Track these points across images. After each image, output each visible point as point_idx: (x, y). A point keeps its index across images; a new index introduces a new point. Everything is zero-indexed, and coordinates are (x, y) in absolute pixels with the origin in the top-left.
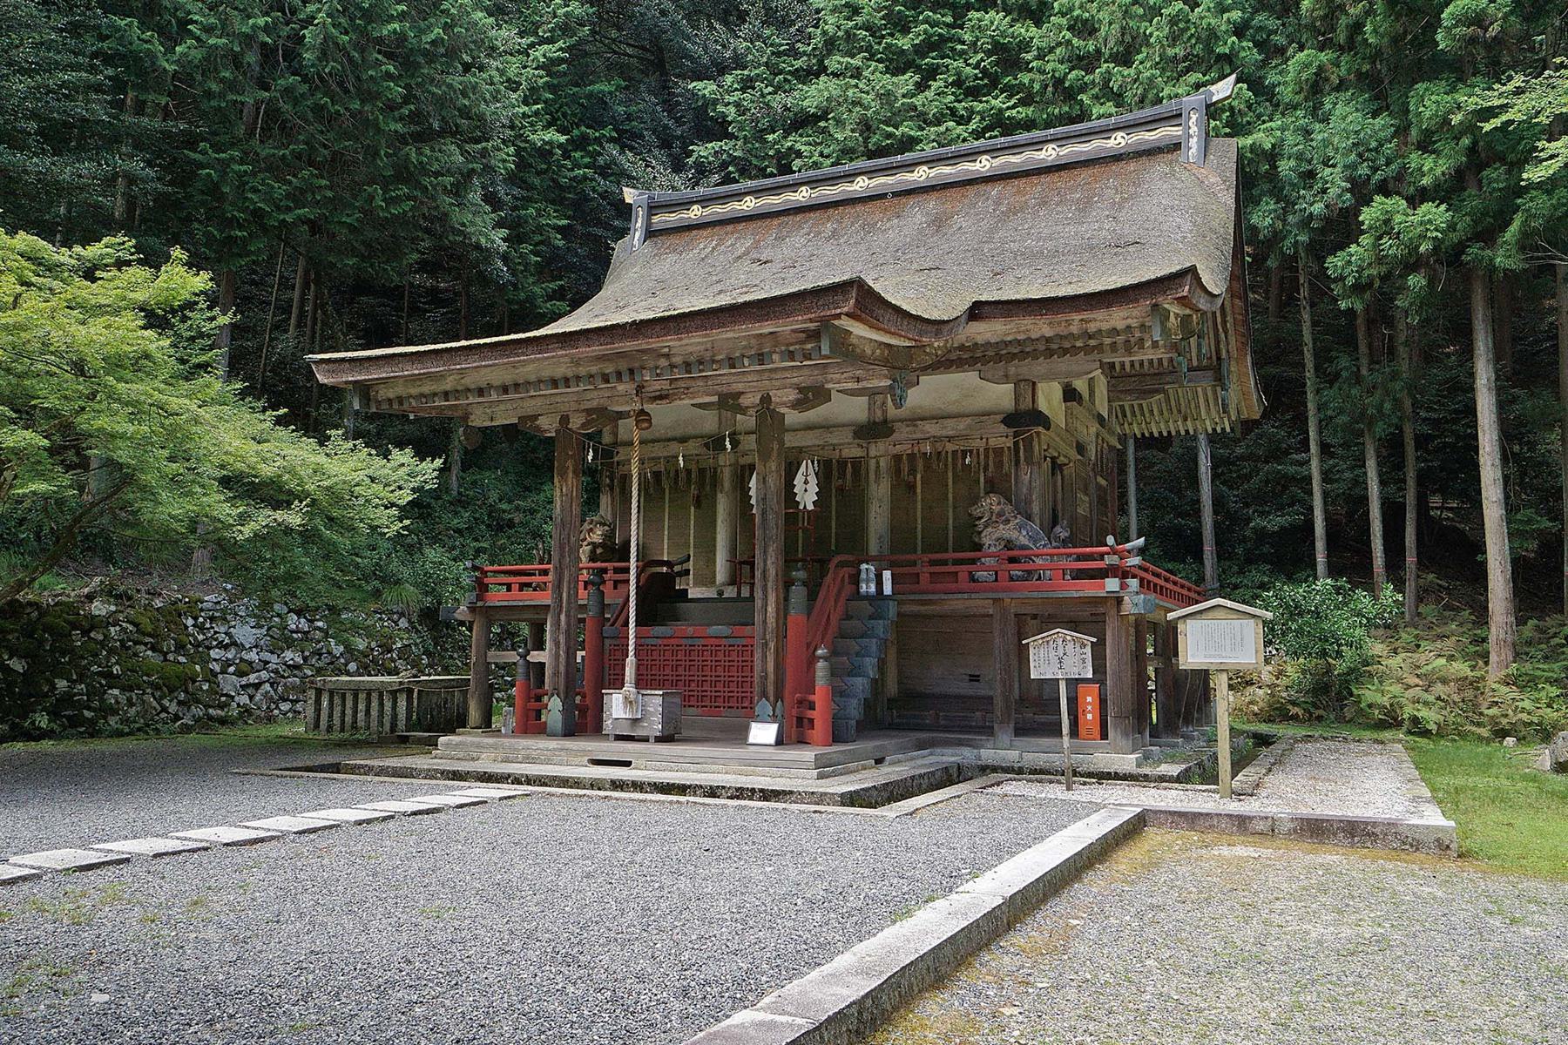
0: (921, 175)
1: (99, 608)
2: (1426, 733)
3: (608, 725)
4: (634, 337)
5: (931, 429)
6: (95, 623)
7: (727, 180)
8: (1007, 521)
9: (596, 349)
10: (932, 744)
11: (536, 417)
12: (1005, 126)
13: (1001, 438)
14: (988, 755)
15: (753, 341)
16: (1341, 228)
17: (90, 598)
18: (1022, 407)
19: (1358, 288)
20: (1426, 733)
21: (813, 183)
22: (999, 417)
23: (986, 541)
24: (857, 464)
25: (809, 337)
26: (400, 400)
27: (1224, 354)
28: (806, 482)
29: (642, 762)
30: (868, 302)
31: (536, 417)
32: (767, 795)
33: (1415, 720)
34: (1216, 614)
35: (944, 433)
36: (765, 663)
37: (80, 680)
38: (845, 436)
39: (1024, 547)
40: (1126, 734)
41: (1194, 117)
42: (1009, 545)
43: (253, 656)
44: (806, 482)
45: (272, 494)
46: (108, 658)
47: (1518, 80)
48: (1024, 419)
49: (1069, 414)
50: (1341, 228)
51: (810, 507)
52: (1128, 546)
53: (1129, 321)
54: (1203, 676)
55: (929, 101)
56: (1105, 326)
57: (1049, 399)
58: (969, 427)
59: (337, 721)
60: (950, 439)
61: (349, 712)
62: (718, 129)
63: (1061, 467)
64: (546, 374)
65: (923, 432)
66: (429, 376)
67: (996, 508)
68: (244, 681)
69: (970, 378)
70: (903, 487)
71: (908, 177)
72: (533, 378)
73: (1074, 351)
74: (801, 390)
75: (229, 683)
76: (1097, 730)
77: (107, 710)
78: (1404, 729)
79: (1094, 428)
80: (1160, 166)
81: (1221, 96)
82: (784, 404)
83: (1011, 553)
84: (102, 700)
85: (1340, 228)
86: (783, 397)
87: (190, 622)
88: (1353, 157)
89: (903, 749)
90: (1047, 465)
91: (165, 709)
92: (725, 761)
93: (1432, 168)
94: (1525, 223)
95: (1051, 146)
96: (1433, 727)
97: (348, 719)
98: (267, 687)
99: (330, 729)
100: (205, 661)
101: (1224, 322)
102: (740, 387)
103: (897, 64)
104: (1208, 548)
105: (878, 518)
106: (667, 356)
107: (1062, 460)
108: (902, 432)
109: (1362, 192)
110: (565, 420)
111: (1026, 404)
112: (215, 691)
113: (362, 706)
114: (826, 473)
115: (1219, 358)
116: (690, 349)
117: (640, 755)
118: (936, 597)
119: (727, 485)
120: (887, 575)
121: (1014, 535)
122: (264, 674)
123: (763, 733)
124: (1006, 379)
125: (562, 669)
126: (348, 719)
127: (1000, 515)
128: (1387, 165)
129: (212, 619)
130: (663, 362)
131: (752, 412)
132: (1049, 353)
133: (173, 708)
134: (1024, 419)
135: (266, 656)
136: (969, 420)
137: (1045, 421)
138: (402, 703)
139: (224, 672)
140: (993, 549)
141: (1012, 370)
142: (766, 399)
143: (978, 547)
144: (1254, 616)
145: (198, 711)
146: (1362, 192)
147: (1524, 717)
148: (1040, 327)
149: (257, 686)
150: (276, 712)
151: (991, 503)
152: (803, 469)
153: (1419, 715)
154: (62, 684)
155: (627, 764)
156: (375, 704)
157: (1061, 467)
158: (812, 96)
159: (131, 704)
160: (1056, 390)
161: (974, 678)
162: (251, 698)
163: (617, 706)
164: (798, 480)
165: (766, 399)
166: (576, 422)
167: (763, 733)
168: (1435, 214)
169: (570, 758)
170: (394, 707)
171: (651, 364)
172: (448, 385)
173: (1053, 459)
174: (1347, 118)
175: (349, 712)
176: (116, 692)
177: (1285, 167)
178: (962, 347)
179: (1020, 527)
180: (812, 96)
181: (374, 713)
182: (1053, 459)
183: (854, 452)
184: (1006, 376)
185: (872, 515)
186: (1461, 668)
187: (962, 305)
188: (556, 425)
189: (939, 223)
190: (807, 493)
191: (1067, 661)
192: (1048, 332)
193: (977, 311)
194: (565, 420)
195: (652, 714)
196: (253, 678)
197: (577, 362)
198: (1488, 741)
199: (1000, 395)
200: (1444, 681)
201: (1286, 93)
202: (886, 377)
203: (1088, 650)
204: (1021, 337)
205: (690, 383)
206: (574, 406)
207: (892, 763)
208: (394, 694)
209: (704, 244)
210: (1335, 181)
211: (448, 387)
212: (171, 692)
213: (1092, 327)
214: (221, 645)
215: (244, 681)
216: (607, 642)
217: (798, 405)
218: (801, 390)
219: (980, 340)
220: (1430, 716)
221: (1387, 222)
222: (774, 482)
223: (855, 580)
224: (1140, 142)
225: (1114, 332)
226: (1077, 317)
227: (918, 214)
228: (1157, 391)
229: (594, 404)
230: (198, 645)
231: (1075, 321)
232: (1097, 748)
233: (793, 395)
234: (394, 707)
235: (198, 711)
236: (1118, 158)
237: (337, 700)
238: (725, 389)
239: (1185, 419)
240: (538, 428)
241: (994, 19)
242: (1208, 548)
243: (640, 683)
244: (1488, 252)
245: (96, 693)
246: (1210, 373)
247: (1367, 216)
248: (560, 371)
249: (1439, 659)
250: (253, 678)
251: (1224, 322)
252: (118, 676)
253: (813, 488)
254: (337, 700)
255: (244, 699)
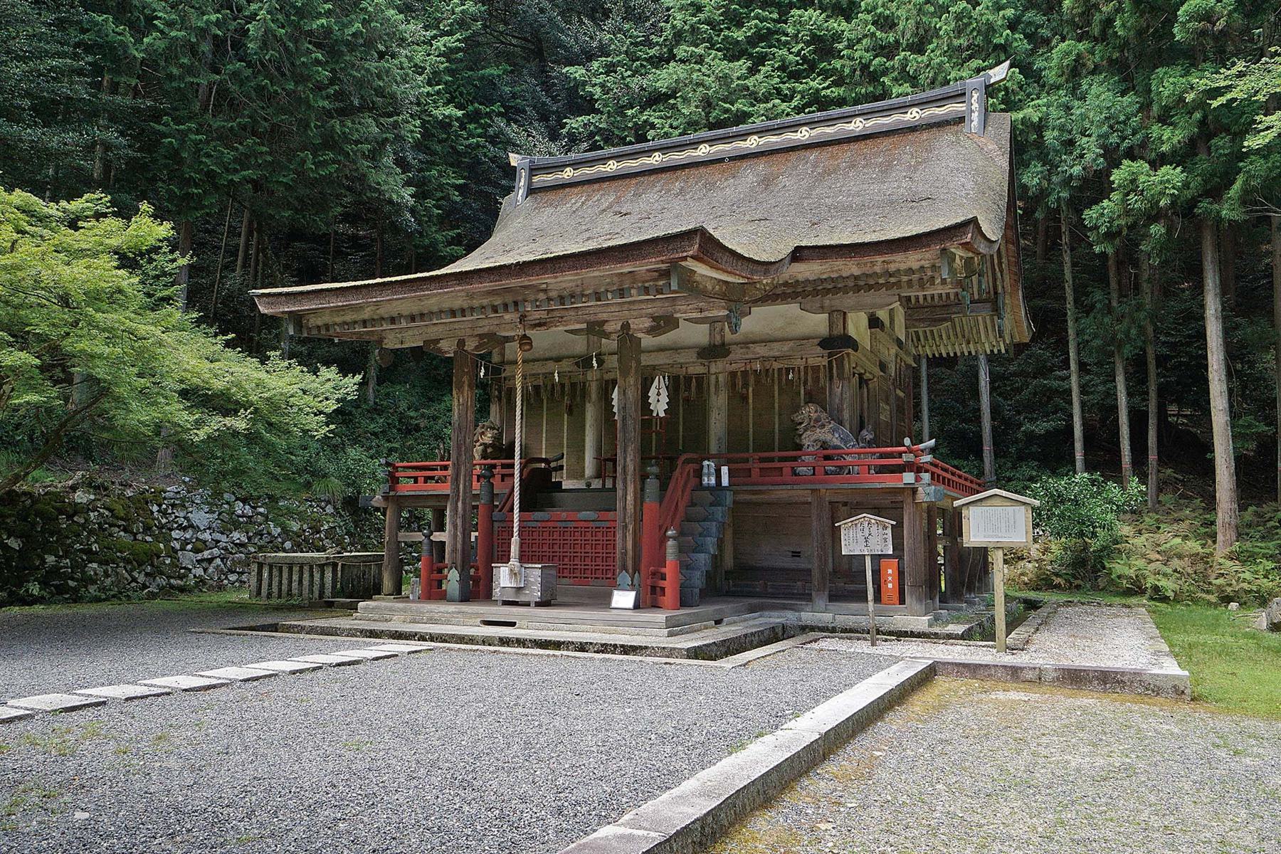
0: (753, 143)
1: (81, 497)
2: (1165, 599)
3: (497, 593)
4: (518, 275)
5: (761, 350)
6: (77, 509)
7: (594, 147)
8: (823, 426)
9: (487, 285)
10: (761, 608)
11: (438, 341)
12: (821, 103)
13: (818, 358)
14: (807, 617)
15: (615, 279)
16: (1096, 186)
17: (74, 488)
18: (835, 333)
19: (1110, 236)
20: (1165, 599)
21: (664, 149)
22: (817, 341)
23: (806, 442)
24: (700, 379)
25: (661, 275)
26: (327, 327)
27: (1000, 290)
28: (659, 394)
29: (524, 623)
30: (709, 247)
31: (438, 341)
32: (627, 650)
33: (1156, 589)
34: (994, 501)
35: (772, 354)
36: (625, 542)
37: (66, 556)
38: (690, 357)
39: (836, 447)
40: (920, 600)
41: (975, 96)
42: (824, 445)
43: (206, 536)
44: (659, 394)
45: (222, 403)
46: (88, 538)
47: (1240, 66)
48: (837, 342)
49: (873, 338)
50: (1096, 186)
51: (662, 414)
52: (922, 446)
53: (923, 262)
54: (983, 552)
55: (759, 82)
56: (903, 267)
57: (857, 326)
58: (792, 349)
59: (275, 589)
60: (776, 358)
61: (285, 582)
62: (587, 106)
63: (867, 381)
64: (446, 306)
65: (754, 353)
66: (351, 307)
67: (814, 415)
68: (199, 556)
69: (792, 309)
70: (738, 398)
71: (742, 144)
72: (435, 309)
73: (877, 287)
74: (654, 319)
75: (187, 558)
76: (896, 597)
77: (88, 581)
78: (1147, 596)
79: (894, 349)
80: (947, 136)
81: (998, 79)
82: (640, 330)
83: (826, 452)
84: (83, 572)
85: (1095, 186)
86: (640, 324)
87: (155, 508)
88: (1105, 128)
89: (738, 612)
90: (855, 380)
91: (134, 580)
92: (593, 622)
93: (1170, 137)
94: (1246, 182)
95: (859, 119)
96: (1170, 594)
97: (285, 588)
98: (218, 561)
99: (269, 595)
100: (168, 540)
101: (1000, 263)
102: (605, 316)
103: (733, 52)
104: (987, 448)
105: (717, 423)
106: (545, 291)
107: (868, 376)
108: (737, 353)
109: (1113, 157)
110: (461, 343)
111: (838, 330)
112: (176, 564)
113: (295, 577)
114: (675, 386)
115: (996, 293)
116: (564, 285)
117: (523, 617)
118: (765, 488)
119: (594, 396)
120: (725, 470)
121: (828, 437)
122: (216, 551)
123: (624, 599)
124: (822, 309)
125: (459, 547)
126: (285, 588)
127: (817, 421)
128: (1133, 135)
129: (173, 506)
130: (542, 296)
131: (614, 336)
132: (857, 289)
133: (141, 578)
134: (837, 342)
135: (217, 536)
136: (791, 343)
137: (854, 344)
138: (329, 575)
139: (183, 549)
140: (811, 449)
141: (827, 303)
142: (626, 326)
143: (799, 447)
144: (1025, 504)
145: (162, 581)
146: (1113, 157)
147: (1245, 586)
148: (850, 267)
149: (210, 561)
150: (226, 582)
151: (810, 411)
152: (656, 383)
153: (1159, 584)
154: (50, 559)
155: (513, 624)
156: (306, 575)
157: (867, 381)
158: (664, 78)
159: (107, 575)
160: (863, 319)
161: (796, 554)
162: (205, 570)
163: (504, 577)
164: (652, 393)
165: (626, 326)
166: (470, 345)
167: (624, 599)
168: (1172, 175)
169: (466, 620)
170: (322, 578)
171: (532, 297)
172: (366, 314)
173: (860, 375)
174: (1101, 96)
175: (285, 582)
176: (95, 565)
177: (1050, 136)
178: (786, 284)
179: (833, 431)
180: (664, 78)
181: (306, 583)
182: (860, 375)
183: (698, 369)
184: (822, 307)
185: (713, 421)
186: (1194, 546)
187: (786, 249)
188: (454, 347)
189: (767, 182)
190: (659, 403)
191: (872, 540)
192: (856, 271)
193: (798, 254)
194: (461, 343)
195: (533, 583)
196: (206, 554)
197: (471, 296)
198: (1216, 606)
199: (817, 323)
200: (1180, 557)
201: (1051, 76)
202: (724, 308)
203: (889, 531)
204: (834, 275)
205: (563, 313)
206: (469, 332)
207: (729, 624)
208: (322, 567)
209: (575, 199)
210: (1091, 148)
211: (366, 317)
212: (140, 565)
213: (892, 268)
214: (181, 527)
215: (199, 556)
216: (496, 525)
217: (652, 331)
218: (654, 319)
219: (800, 278)
220: (1169, 585)
221: (1133, 181)
222: (633, 394)
223: (699, 474)
224: (931, 116)
225: (910, 271)
226: (879, 259)
227: (750, 175)
228: (945, 320)
229: (486, 330)
230: (161, 527)
231: (878, 263)
232: (896, 611)
233: (648, 323)
234: (322, 578)
235: (162, 581)
236: (913, 129)
237: (275, 572)
238: (592, 318)
239: (968, 343)
240: (440, 350)
241: (812, 15)
242: (987, 448)
243: (523, 558)
244: (1216, 206)
245: (78, 566)
246: (989, 305)
247: (1117, 176)
248: (458, 303)
249: (1176, 538)
250: (206, 554)
251: (1000, 263)
252: (96, 553)
253: (664, 399)
254: (275, 572)
255: (200, 572)
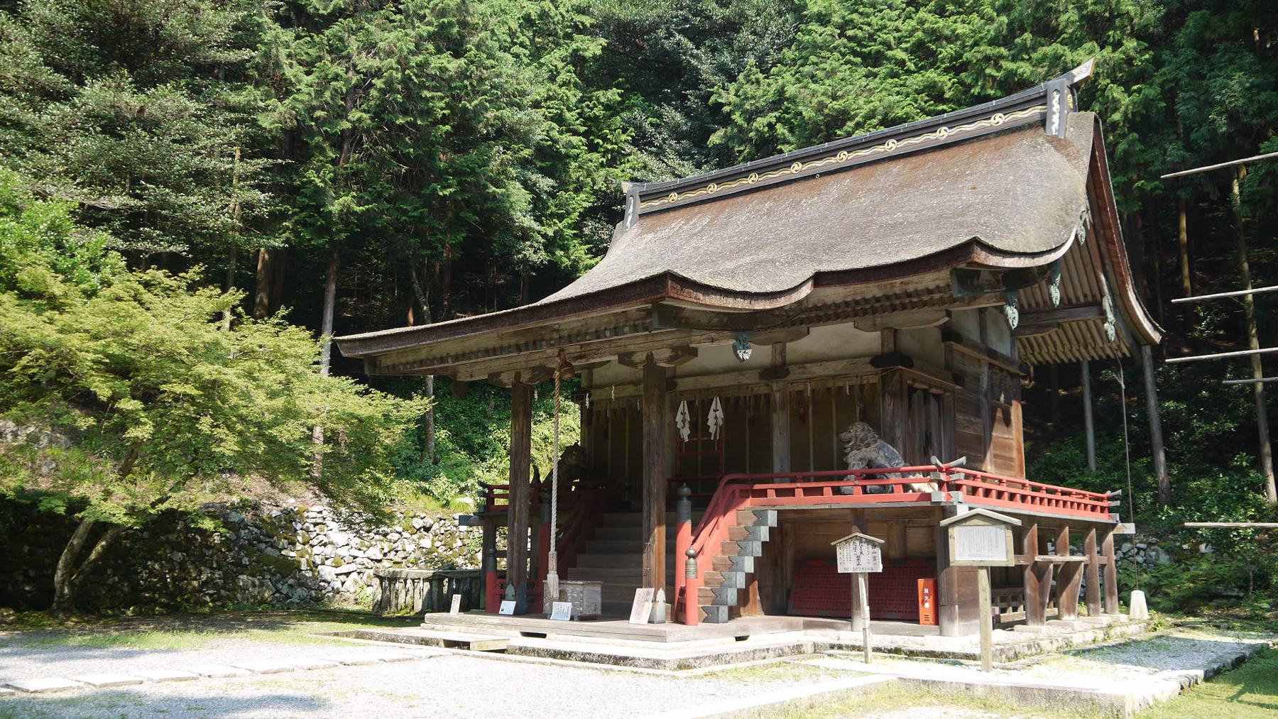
0: (844, 158)
4: (530, 319)
5: (817, 370)
11: (499, 374)
21: (850, 148)
22: (868, 359)
24: (767, 396)
26: (394, 366)
31: (499, 374)
32: (618, 660)
42: (870, 464)
43: (344, 552)
46: (238, 552)
53: (938, 282)
56: (920, 287)
60: (833, 377)
64: (483, 346)
68: (338, 571)
69: (847, 327)
71: (932, 136)
72: (475, 349)
74: (674, 349)
76: (931, 616)
82: (662, 360)
83: (871, 471)
95: (891, 141)
102: (632, 348)
106: (557, 331)
108: (795, 373)
110: (518, 375)
116: (572, 325)
117: (552, 629)
121: (873, 455)
124: (874, 328)
125: (515, 563)
129: (315, 524)
130: (556, 336)
131: (641, 367)
133: (285, 590)
136: (844, 363)
139: (323, 564)
141: (879, 321)
142: (650, 357)
144: (1004, 523)
148: (871, 290)
149: (348, 574)
151: (858, 430)
152: (713, 406)
155: (544, 636)
165: (650, 357)
166: (525, 377)
169: (603, 639)
171: (548, 337)
176: (245, 577)
183: (763, 390)
184: (874, 325)
185: (775, 444)
188: (512, 379)
191: (863, 559)
192: (879, 294)
193: (819, 279)
194: (518, 375)
197: (501, 337)
202: (731, 338)
204: (859, 298)
205: (600, 346)
206: (524, 365)
211: (423, 357)
212: (284, 577)
213: (911, 288)
218: (674, 349)
219: (829, 301)
224: (1015, 120)
226: (898, 281)
229: (536, 363)
231: (896, 285)
232: (929, 632)
238: (622, 350)
240: (501, 382)
250: (344, 569)
252: (246, 566)
